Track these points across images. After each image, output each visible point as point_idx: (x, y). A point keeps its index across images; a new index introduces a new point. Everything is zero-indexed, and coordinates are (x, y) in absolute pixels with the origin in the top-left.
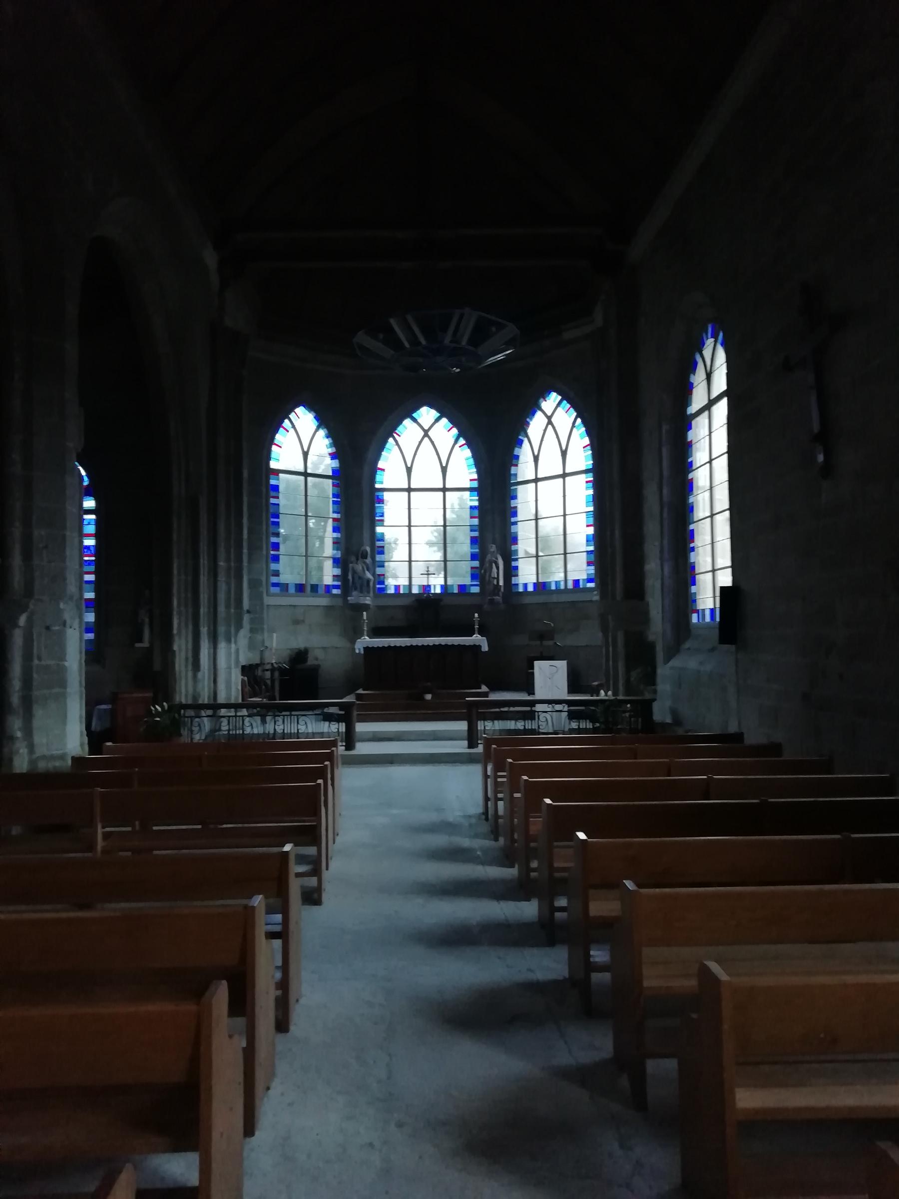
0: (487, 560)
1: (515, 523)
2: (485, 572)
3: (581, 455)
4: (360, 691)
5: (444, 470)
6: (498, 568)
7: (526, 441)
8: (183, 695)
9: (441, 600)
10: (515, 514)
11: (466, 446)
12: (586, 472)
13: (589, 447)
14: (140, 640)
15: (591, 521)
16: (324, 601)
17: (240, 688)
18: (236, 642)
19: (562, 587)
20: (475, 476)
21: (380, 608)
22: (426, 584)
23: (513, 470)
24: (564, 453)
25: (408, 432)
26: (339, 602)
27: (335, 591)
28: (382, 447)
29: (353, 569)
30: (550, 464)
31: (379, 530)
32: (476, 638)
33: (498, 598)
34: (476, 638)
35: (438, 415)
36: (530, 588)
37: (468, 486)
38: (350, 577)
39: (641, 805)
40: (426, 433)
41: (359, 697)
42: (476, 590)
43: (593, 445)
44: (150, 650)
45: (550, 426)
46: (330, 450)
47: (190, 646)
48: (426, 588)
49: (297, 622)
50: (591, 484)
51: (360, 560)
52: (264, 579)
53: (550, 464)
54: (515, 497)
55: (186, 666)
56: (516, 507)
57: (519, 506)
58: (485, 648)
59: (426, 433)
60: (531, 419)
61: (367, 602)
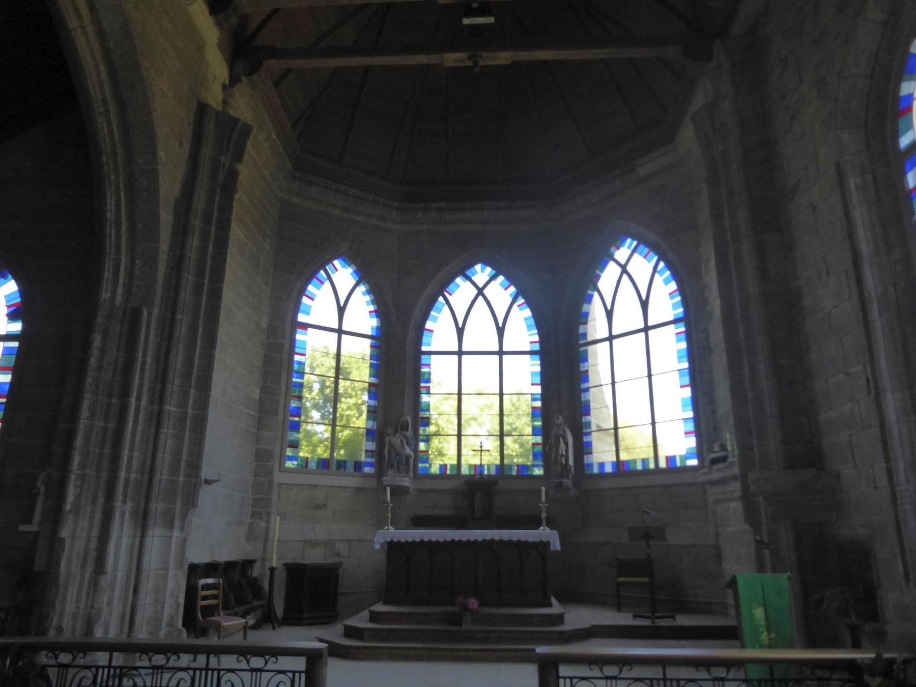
0: (553, 434)
1: (587, 390)
2: (550, 449)
3: (666, 301)
4: (380, 608)
5: (501, 331)
6: (567, 444)
7: (596, 294)
8: (65, 619)
9: (496, 483)
10: (586, 380)
11: (525, 305)
12: (676, 321)
13: (677, 293)
14: (29, 521)
15: (687, 380)
16: (352, 482)
17: (182, 600)
18: (182, 528)
19: (652, 466)
20: (536, 338)
21: (421, 491)
22: (478, 463)
23: (581, 329)
24: (645, 304)
25: (461, 293)
26: (373, 483)
27: (367, 470)
28: (430, 305)
29: (389, 442)
30: (628, 315)
31: (425, 398)
32: (544, 533)
33: (567, 482)
34: (544, 533)
35: (494, 272)
36: (609, 469)
37: (528, 349)
38: (386, 453)
39: (489, 544)
40: (480, 291)
41: (375, 617)
42: (538, 472)
43: (681, 290)
44: (36, 535)
45: (625, 276)
46: (372, 308)
47: (95, 533)
48: (479, 468)
49: (318, 507)
50: (683, 336)
51: (398, 435)
52: (277, 450)
53: (628, 315)
54: (585, 360)
55: (83, 566)
56: (587, 371)
57: (590, 369)
58: (556, 545)
59: (480, 291)
60: (602, 271)
61: (406, 484)
